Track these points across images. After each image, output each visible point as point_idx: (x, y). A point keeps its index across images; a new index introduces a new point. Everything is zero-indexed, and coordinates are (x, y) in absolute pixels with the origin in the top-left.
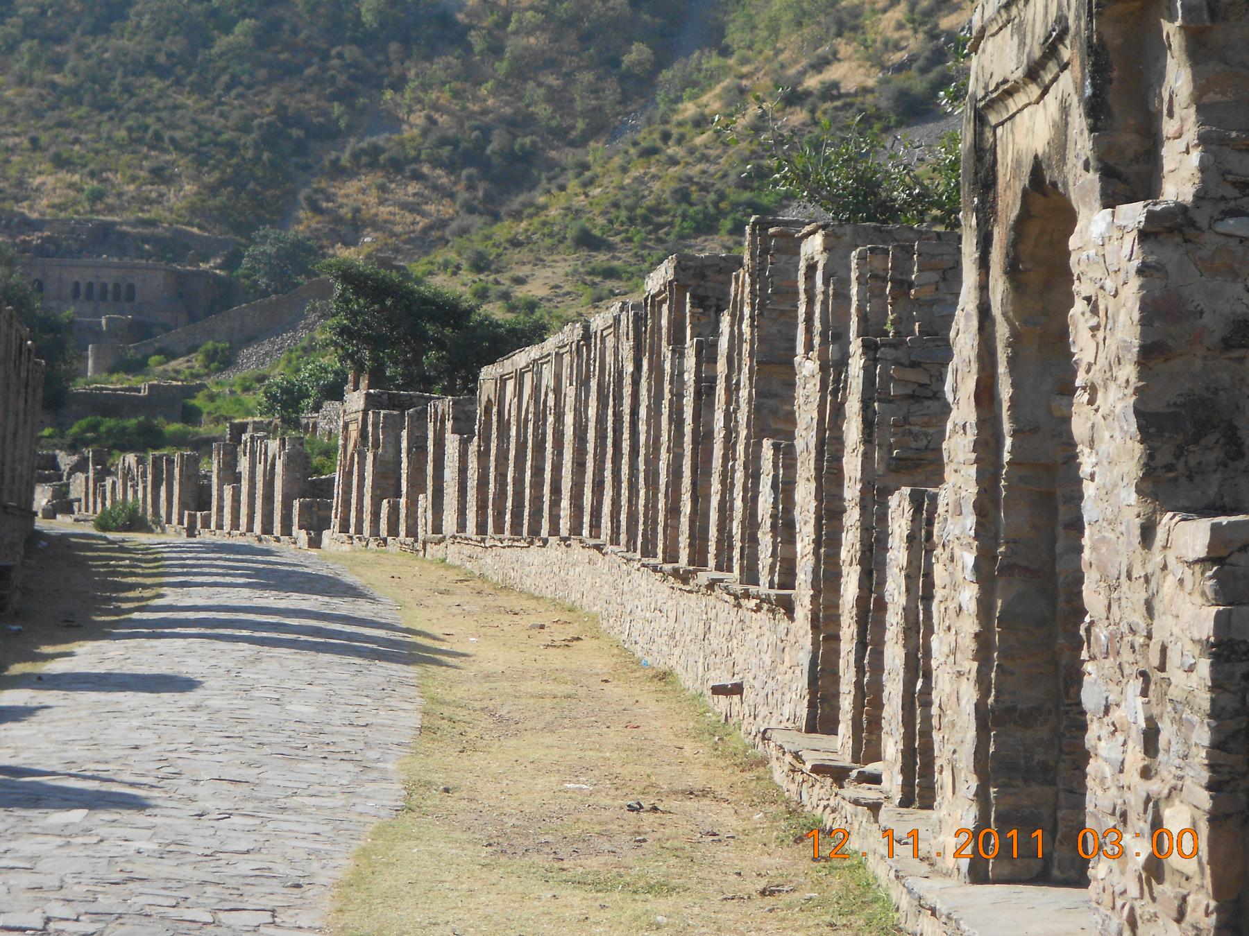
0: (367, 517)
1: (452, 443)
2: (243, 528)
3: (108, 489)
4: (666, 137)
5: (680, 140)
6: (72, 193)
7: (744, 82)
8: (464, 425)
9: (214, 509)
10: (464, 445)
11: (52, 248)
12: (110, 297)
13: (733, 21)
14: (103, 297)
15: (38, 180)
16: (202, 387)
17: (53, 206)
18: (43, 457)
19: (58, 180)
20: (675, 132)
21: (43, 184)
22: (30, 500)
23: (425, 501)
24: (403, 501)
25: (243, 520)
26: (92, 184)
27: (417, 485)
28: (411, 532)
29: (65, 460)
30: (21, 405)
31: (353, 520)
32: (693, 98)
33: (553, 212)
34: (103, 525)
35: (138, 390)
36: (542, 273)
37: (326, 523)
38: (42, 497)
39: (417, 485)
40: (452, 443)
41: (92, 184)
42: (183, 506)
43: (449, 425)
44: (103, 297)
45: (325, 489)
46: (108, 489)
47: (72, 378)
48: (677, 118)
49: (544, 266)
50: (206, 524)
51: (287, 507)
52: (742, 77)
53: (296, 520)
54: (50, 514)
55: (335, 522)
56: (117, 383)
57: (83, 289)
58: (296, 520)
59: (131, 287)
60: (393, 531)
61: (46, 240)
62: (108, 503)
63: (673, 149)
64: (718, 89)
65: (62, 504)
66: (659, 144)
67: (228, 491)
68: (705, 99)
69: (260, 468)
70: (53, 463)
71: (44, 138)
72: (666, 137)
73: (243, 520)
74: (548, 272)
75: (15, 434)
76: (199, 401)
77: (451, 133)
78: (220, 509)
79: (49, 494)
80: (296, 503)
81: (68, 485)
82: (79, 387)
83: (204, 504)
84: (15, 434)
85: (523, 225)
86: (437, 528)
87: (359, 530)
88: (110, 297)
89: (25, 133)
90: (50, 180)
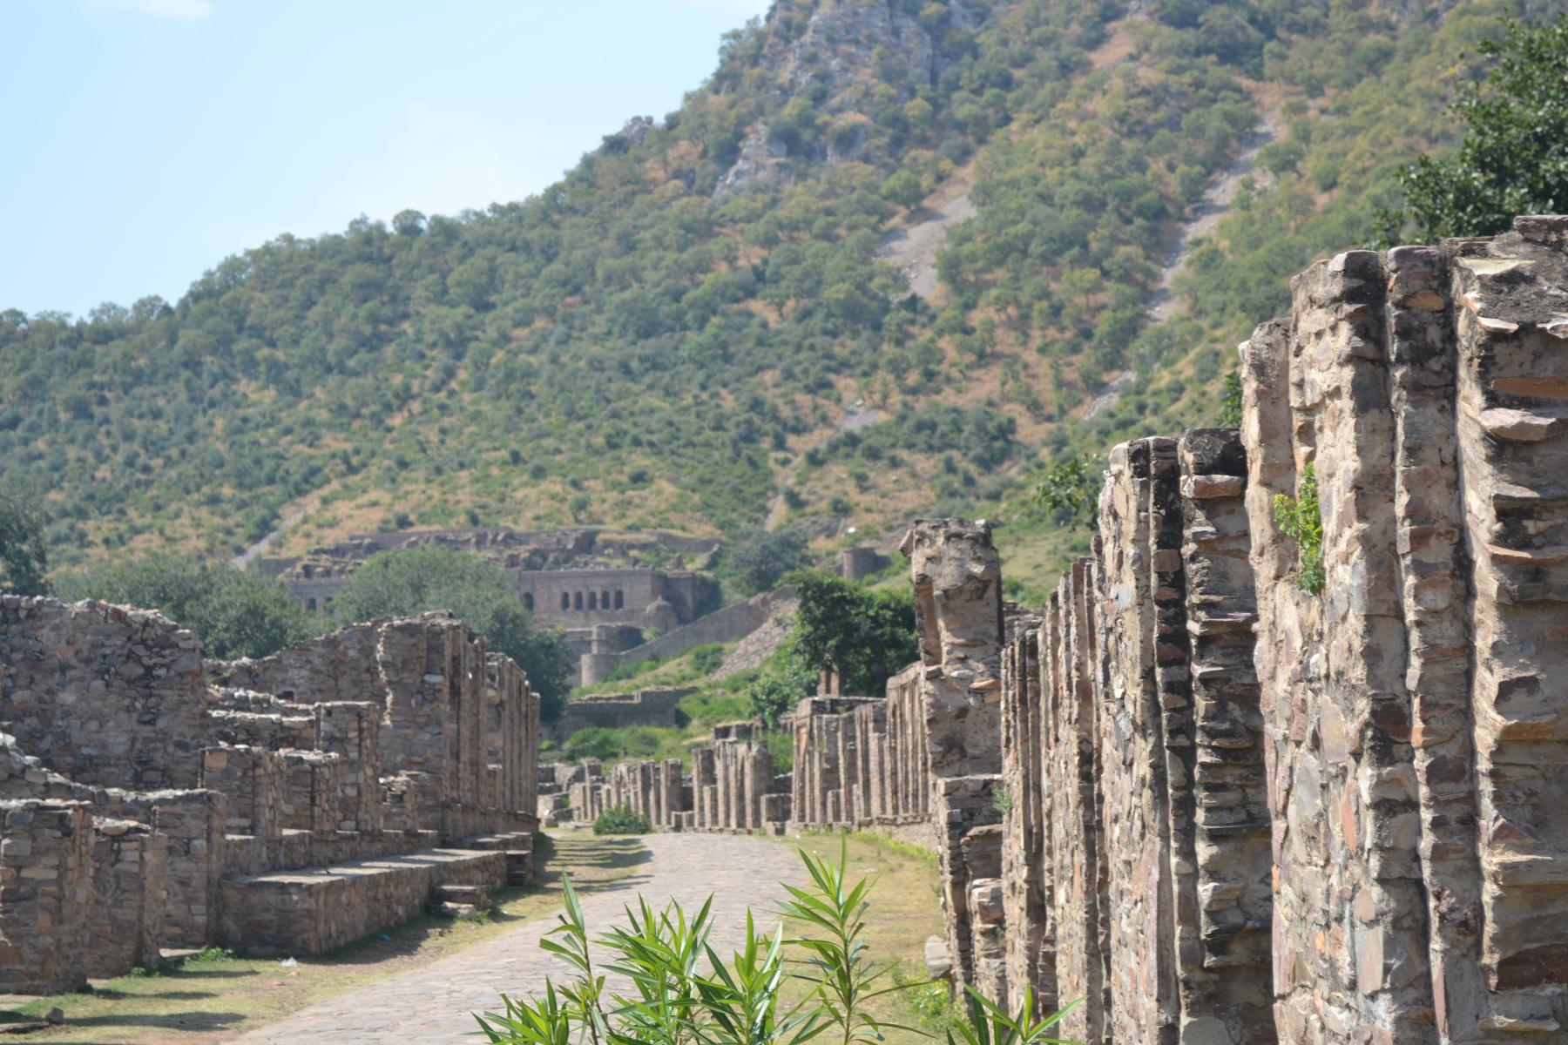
0: (818, 807)
1: (873, 737)
2: (721, 825)
3: (604, 796)
4: (1141, 408)
5: (1155, 412)
6: (557, 505)
7: (1218, 346)
8: (879, 721)
9: (696, 808)
10: (881, 739)
11: (539, 560)
12: (599, 605)
13: (1396, 154)
14: (592, 605)
15: (519, 495)
16: (693, 690)
17: (538, 518)
18: (542, 770)
19: (542, 492)
20: (1151, 401)
21: (526, 496)
22: (534, 810)
23: (857, 790)
24: (842, 791)
25: (721, 816)
26: (574, 495)
27: (851, 779)
28: (850, 817)
29: (564, 772)
30: (523, 733)
31: (808, 811)
32: (1168, 364)
33: (1033, 492)
34: (598, 831)
35: (631, 697)
36: (1023, 553)
37: (786, 815)
38: (544, 808)
39: (851, 779)
40: (873, 737)
41: (574, 495)
42: (671, 807)
43: (871, 726)
44: (592, 605)
45: (785, 785)
46: (604, 796)
47: (567, 689)
48: (1152, 387)
49: (1025, 546)
50: (691, 822)
51: (756, 802)
52: (1215, 341)
53: (764, 812)
54: (552, 824)
55: (795, 814)
56: (610, 692)
57: (572, 599)
58: (764, 812)
59: (619, 595)
60: (837, 817)
61: (535, 552)
62: (605, 808)
63: (1149, 420)
64: (1192, 355)
65: (563, 812)
66: (1135, 415)
67: (707, 790)
68: (1179, 366)
69: (732, 769)
70: (550, 775)
71: (525, 452)
72: (1141, 408)
73: (721, 816)
74: (1029, 552)
75: (520, 757)
76: (686, 705)
77: (926, 417)
78: (702, 808)
79: (551, 805)
80: (764, 799)
81: (567, 796)
82: (574, 698)
83: (688, 805)
84: (520, 757)
85: (1004, 505)
86: (868, 812)
87: (813, 819)
88: (599, 605)
89: (505, 447)
90: (532, 492)
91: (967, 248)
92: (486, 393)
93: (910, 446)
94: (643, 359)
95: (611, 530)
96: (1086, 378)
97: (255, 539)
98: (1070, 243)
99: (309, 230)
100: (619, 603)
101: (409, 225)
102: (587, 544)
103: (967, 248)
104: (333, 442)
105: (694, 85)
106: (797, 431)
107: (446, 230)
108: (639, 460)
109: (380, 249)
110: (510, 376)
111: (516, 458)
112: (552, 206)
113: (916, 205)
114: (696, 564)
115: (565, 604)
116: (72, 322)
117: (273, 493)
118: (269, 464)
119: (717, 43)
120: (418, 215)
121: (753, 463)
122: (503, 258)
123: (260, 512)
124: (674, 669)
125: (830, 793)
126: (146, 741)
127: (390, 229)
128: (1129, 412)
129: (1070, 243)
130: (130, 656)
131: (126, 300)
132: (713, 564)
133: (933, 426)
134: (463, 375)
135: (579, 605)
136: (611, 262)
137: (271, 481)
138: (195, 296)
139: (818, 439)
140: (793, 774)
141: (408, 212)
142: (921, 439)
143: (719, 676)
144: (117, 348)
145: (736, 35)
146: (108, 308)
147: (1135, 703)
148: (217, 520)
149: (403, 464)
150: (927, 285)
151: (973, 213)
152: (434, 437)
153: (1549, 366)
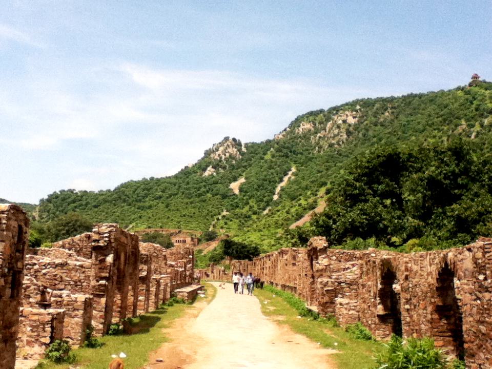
59: (185, 241)
93: (233, 218)
99: (136, 179)
101: (152, 179)
107: (158, 180)
109: (405, 224)
112: (176, 176)
113: (235, 179)
125: (490, 246)
126: (157, 267)
127: (149, 179)
128: (270, 214)
130: (154, 252)
131: (105, 189)
133: (237, 215)
138: (115, 189)
140: (115, 286)
142: (235, 217)
150: (237, 192)
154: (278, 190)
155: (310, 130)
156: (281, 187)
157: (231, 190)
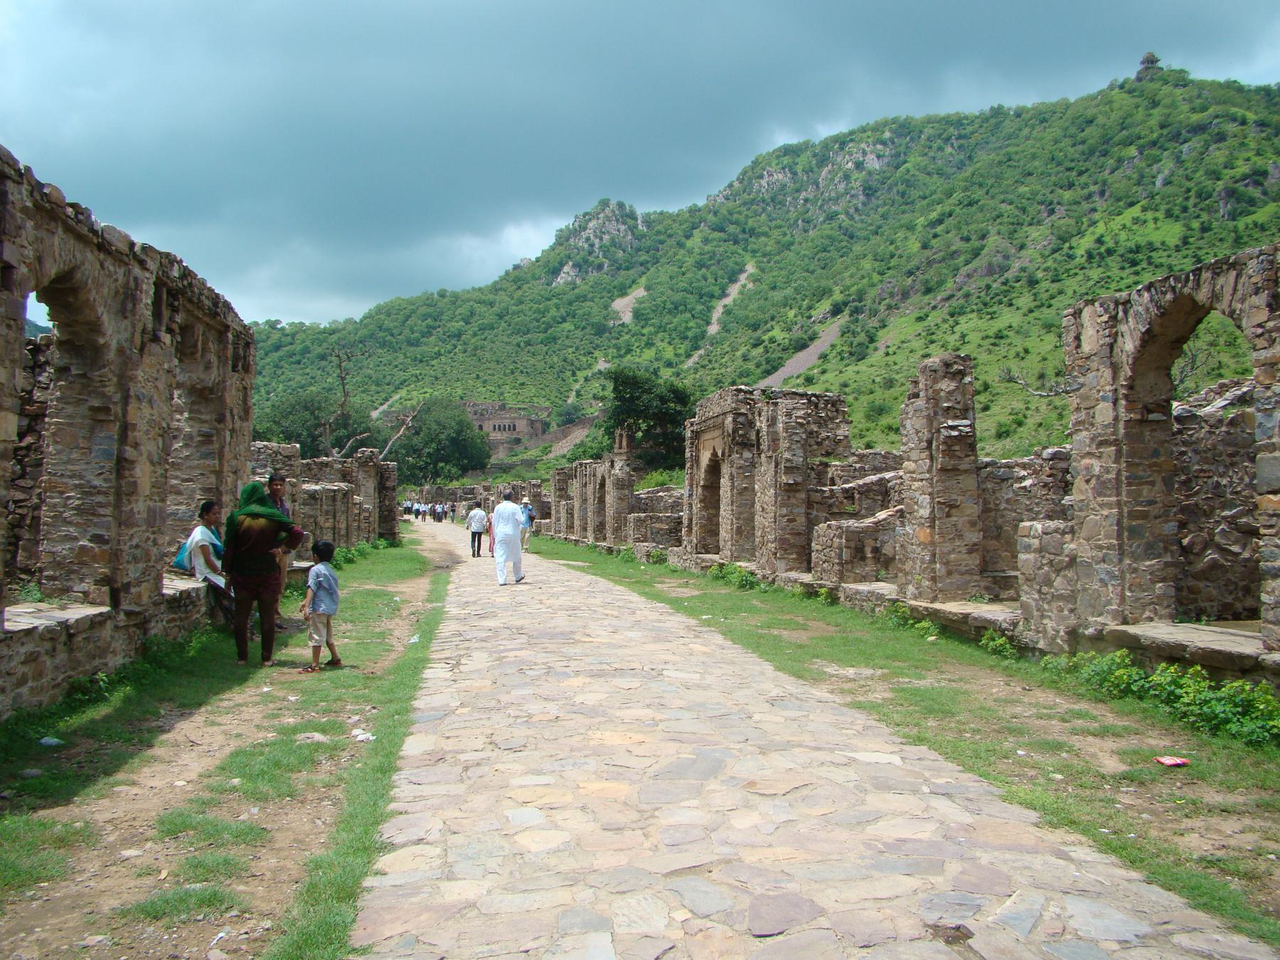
14: (505, 430)
41: (498, 391)
59: (514, 426)
71: (481, 374)
91: (643, 306)
92: (467, 354)
94: (525, 342)
95: (511, 403)
96: (686, 352)
97: (382, 404)
98: (676, 308)
100: (514, 429)
102: (503, 407)
103: (643, 306)
104: (412, 371)
105: (546, 247)
106: (579, 370)
108: (522, 379)
110: (476, 349)
111: (478, 377)
113: (623, 291)
114: (543, 415)
115: (495, 429)
116: (322, 327)
117: (391, 388)
118: (388, 378)
119: (554, 233)
120: (445, 291)
121: (564, 380)
122: (476, 305)
123: (383, 395)
124: (532, 454)
129: (676, 308)
132: (549, 416)
134: (459, 347)
135: (499, 429)
136: (514, 308)
137: (388, 384)
138: (365, 318)
139: (589, 373)
141: (441, 290)
143: (551, 456)
144: (334, 338)
145: (561, 230)
146: (335, 322)
147: (1128, 356)
148: (370, 398)
149: (437, 378)
150: (627, 318)
151: (645, 294)
152: (448, 369)
153: (1278, 107)
154: (717, 313)
155: (784, 186)
156: (725, 306)
157: (616, 315)
